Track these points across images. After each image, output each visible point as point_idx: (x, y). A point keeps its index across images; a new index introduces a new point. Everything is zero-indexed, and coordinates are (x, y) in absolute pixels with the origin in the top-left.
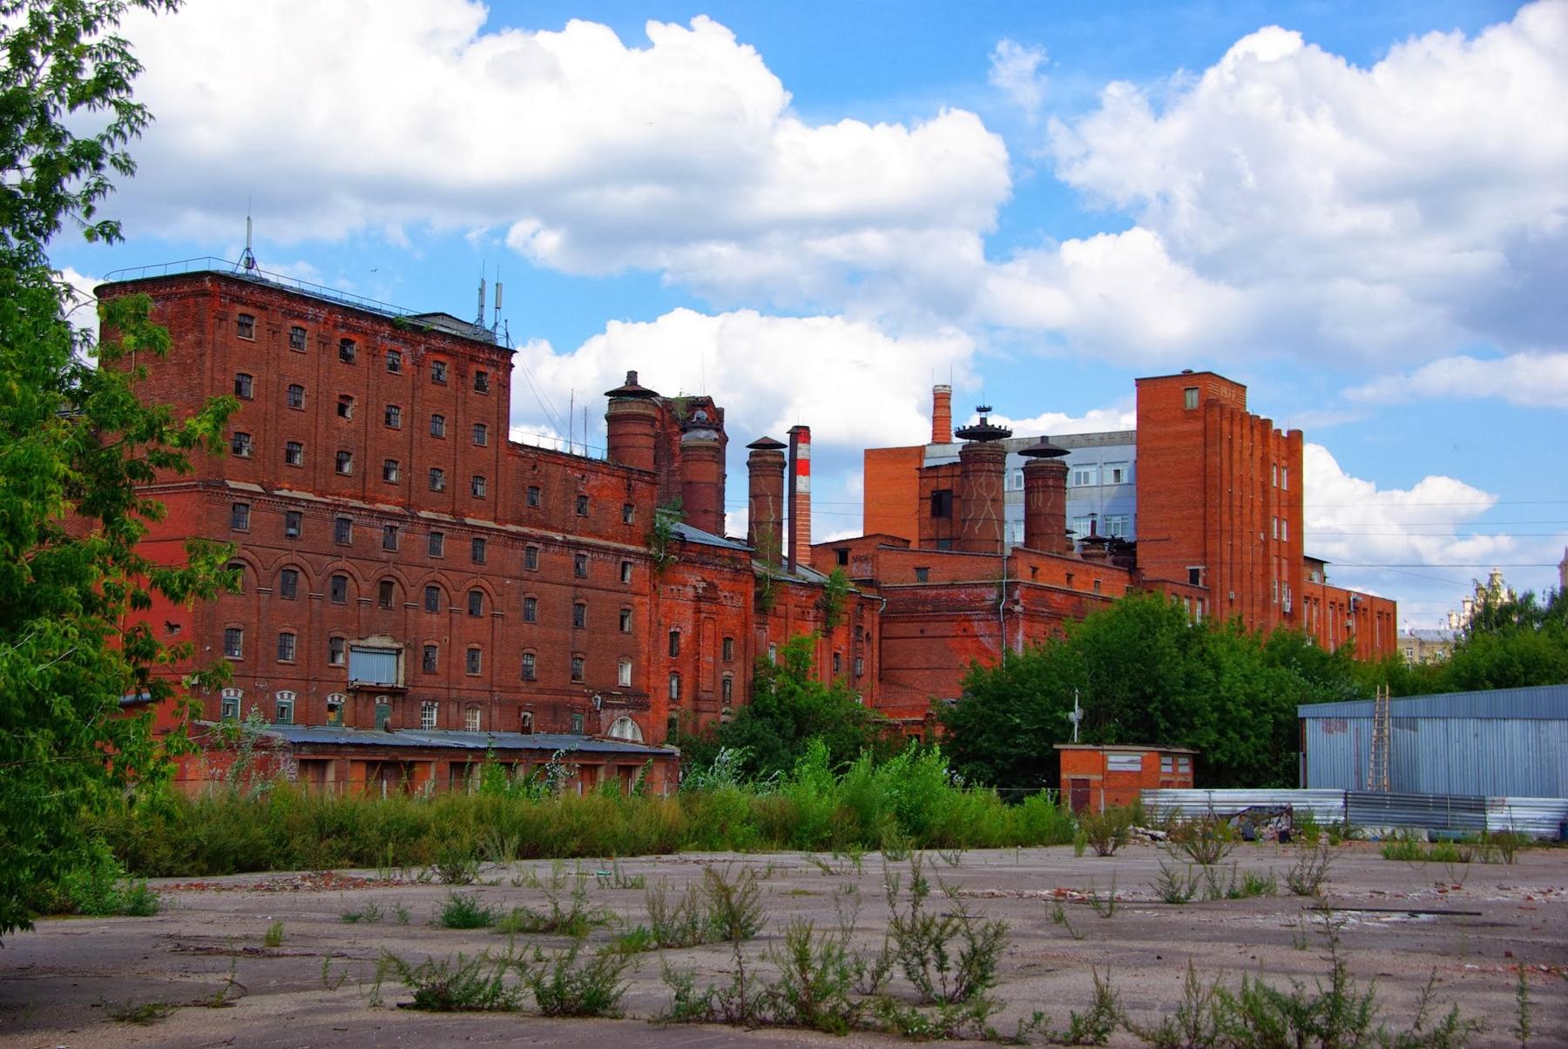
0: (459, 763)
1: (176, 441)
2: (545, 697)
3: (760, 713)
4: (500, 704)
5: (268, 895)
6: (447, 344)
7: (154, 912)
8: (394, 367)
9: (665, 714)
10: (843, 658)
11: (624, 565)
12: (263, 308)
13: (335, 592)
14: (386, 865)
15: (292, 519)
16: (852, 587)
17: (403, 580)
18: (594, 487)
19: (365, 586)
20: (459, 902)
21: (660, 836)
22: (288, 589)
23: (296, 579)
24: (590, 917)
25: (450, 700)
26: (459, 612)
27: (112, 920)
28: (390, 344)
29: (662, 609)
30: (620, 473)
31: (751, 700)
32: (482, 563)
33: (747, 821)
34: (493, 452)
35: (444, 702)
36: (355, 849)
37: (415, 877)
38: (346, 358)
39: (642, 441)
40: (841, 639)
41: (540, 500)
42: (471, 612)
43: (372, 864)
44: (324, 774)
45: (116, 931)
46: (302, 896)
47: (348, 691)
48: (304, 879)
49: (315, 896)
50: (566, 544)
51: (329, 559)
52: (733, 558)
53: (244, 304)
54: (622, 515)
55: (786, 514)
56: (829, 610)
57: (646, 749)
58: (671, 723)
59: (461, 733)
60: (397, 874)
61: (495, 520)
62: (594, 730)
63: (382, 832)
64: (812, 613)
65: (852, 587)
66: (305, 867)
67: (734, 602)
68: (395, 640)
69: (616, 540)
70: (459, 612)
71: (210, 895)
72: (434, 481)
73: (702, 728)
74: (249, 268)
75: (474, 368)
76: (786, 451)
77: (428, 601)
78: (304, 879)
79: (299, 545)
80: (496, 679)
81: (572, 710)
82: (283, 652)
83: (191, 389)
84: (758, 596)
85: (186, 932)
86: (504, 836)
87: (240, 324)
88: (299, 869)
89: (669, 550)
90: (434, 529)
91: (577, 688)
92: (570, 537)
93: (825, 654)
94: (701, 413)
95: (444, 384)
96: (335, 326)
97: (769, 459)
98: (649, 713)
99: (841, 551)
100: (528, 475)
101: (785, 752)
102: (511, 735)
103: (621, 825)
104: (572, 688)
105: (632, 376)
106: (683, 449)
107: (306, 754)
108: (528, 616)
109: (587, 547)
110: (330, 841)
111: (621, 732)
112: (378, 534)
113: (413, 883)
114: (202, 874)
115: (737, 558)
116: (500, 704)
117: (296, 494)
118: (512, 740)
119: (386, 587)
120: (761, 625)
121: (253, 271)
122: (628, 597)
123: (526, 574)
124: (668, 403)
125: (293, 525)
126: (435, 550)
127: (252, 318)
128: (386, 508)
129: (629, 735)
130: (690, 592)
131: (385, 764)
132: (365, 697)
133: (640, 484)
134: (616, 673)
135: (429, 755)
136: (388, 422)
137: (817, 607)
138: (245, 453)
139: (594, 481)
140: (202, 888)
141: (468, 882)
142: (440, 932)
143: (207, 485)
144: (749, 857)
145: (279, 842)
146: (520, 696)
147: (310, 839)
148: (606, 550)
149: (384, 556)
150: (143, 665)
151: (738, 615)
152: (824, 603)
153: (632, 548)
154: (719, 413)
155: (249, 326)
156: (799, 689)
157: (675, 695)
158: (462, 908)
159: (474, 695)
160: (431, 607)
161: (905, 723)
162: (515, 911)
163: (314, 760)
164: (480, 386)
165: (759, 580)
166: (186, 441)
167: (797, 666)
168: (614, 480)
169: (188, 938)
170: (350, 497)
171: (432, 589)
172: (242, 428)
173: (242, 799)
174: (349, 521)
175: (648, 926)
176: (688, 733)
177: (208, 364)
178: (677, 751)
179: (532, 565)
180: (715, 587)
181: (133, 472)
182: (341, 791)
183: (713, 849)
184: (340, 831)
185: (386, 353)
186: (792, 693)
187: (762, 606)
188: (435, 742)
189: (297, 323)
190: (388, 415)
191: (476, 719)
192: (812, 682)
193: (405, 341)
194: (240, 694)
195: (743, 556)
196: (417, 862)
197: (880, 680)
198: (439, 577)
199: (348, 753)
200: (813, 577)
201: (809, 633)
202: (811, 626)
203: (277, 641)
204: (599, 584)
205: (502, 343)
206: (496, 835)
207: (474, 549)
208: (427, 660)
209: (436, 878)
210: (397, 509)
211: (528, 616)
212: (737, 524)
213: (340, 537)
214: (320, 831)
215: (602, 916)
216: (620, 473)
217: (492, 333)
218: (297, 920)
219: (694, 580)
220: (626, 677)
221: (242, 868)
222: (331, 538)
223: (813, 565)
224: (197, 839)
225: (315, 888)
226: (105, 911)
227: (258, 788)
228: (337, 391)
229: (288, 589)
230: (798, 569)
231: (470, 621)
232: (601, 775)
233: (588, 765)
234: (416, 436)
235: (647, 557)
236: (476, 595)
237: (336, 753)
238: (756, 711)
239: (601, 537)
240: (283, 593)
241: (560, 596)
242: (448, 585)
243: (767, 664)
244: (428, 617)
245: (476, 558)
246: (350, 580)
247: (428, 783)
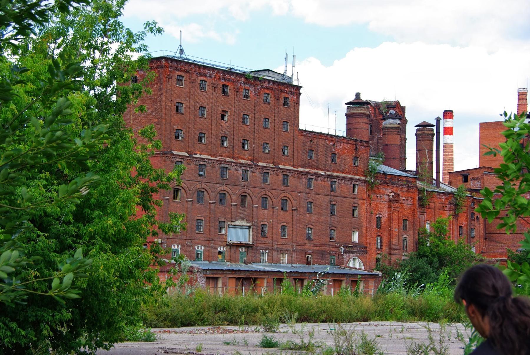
0: (278, 279)
1: (166, 180)
2: (317, 248)
3: (421, 256)
4: (297, 251)
5: (195, 335)
6: (270, 85)
7: (154, 340)
8: (246, 96)
9: (375, 256)
10: (464, 229)
11: (354, 185)
12: (188, 72)
13: (221, 200)
14: (242, 324)
15: (202, 167)
16: (468, 194)
17: (251, 194)
18: (339, 149)
19: (234, 198)
20: (266, 338)
21: (362, 314)
22: (200, 199)
23: (203, 195)
24: (316, 344)
25: (273, 249)
26: (277, 209)
27: (140, 343)
28: (244, 86)
29: (373, 206)
30: (352, 142)
31: (417, 249)
32: (287, 186)
33: (403, 308)
34: (292, 134)
35: (271, 250)
36: (229, 318)
37: (253, 329)
38: (224, 93)
39: (362, 126)
40: (463, 219)
41: (314, 156)
42: (282, 209)
43: (236, 324)
44: (217, 284)
45: (142, 346)
46: (209, 336)
47: (227, 245)
48: (209, 329)
49: (213, 336)
50: (326, 176)
51: (217, 185)
52: (407, 181)
53: (180, 71)
54: (353, 162)
55: (434, 159)
56: (456, 205)
57: (365, 272)
58: (378, 260)
59: (279, 265)
60: (246, 328)
61: (293, 166)
62: (341, 263)
63: (241, 310)
64: (448, 207)
65: (468, 194)
66: (209, 324)
67: (408, 202)
68: (248, 222)
69: (350, 174)
70: (277, 209)
71: (173, 335)
72: (265, 148)
73: (393, 263)
74: (181, 54)
75: (283, 95)
76: (435, 128)
77: (263, 204)
78: (209, 329)
79: (205, 180)
80: (294, 239)
81: (330, 254)
82: (198, 227)
83: (156, 110)
84: (420, 199)
85: (167, 347)
86: (292, 313)
87: (178, 80)
88: (207, 326)
89: (376, 178)
90: (265, 171)
91: (332, 244)
92: (328, 173)
93: (455, 227)
94: (392, 112)
95: (269, 103)
96: (219, 79)
97: (426, 132)
98: (367, 255)
99: (465, 175)
100: (308, 144)
101: (433, 275)
102: (302, 266)
103: (344, 308)
104: (330, 243)
105: (358, 95)
106: (384, 129)
107: (209, 275)
108: (309, 210)
109: (336, 177)
110: (219, 314)
111: (354, 264)
112: (239, 173)
113: (253, 331)
114: (169, 327)
115: (409, 181)
116: (297, 251)
117: (203, 156)
118: (302, 268)
119: (243, 198)
120: (422, 213)
121: (183, 56)
122: (356, 200)
123: (307, 191)
124: (378, 105)
125: (202, 171)
126: (265, 180)
127: (183, 77)
128: (243, 161)
129: (357, 266)
130: (386, 198)
131: (244, 279)
132: (235, 248)
133: (361, 147)
134: (350, 236)
135: (264, 275)
136: (244, 122)
137: (450, 204)
138: (180, 139)
139: (339, 146)
140: (169, 332)
141: (275, 331)
142: (259, 349)
143: (164, 153)
144: (404, 324)
145: (199, 314)
146: (306, 248)
147: (211, 313)
148: (345, 179)
149: (243, 184)
150: (157, 255)
151: (410, 208)
152: (454, 202)
153: (358, 177)
154: (403, 109)
155: (181, 80)
156: (441, 244)
157: (379, 247)
158: (267, 340)
159: (284, 247)
160: (264, 207)
161: (497, 261)
162: (288, 341)
163: (212, 277)
164: (285, 104)
165: (420, 191)
166: (169, 180)
167: (440, 233)
168: (349, 146)
169: (169, 349)
170: (227, 157)
171: (264, 198)
172: (179, 127)
173: (183, 296)
174: (226, 168)
175: (334, 349)
176: (386, 265)
177: (164, 99)
178: (380, 274)
179: (310, 186)
180: (399, 195)
181: (152, 191)
182: (222, 292)
183: (387, 320)
184: (223, 310)
185: (243, 90)
186: (437, 246)
187: (422, 204)
188: (267, 269)
189: (202, 78)
190: (244, 119)
191: (285, 258)
192: (448, 241)
193: (251, 84)
194: (179, 247)
195: (412, 180)
196: (254, 323)
197: (485, 239)
198: (267, 193)
199: (228, 274)
200: (449, 189)
201: (447, 216)
202: (448, 213)
203: (195, 223)
204: (343, 195)
205: (295, 83)
206: (288, 312)
207: (284, 179)
208: (263, 231)
209: (262, 330)
210: (248, 162)
211: (309, 210)
212: (411, 164)
213: (222, 175)
214: (216, 309)
215: (320, 344)
216: (352, 142)
217: (291, 78)
218: (207, 344)
219: (388, 192)
220: (355, 238)
221: (184, 325)
222: (219, 175)
223: (450, 183)
224: (166, 313)
225: (214, 333)
226: (136, 340)
227: (189, 292)
228: (221, 109)
229: (200, 199)
230: (441, 185)
231: (282, 213)
232: (344, 285)
233: (337, 280)
234: (256, 128)
235: (365, 181)
236: (284, 201)
237: (223, 274)
238: (419, 254)
239: (343, 172)
240: (198, 201)
241: (324, 200)
242: (272, 196)
243: (425, 231)
244: (263, 211)
245: (284, 184)
246: (227, 195)
247: (264, 287)
